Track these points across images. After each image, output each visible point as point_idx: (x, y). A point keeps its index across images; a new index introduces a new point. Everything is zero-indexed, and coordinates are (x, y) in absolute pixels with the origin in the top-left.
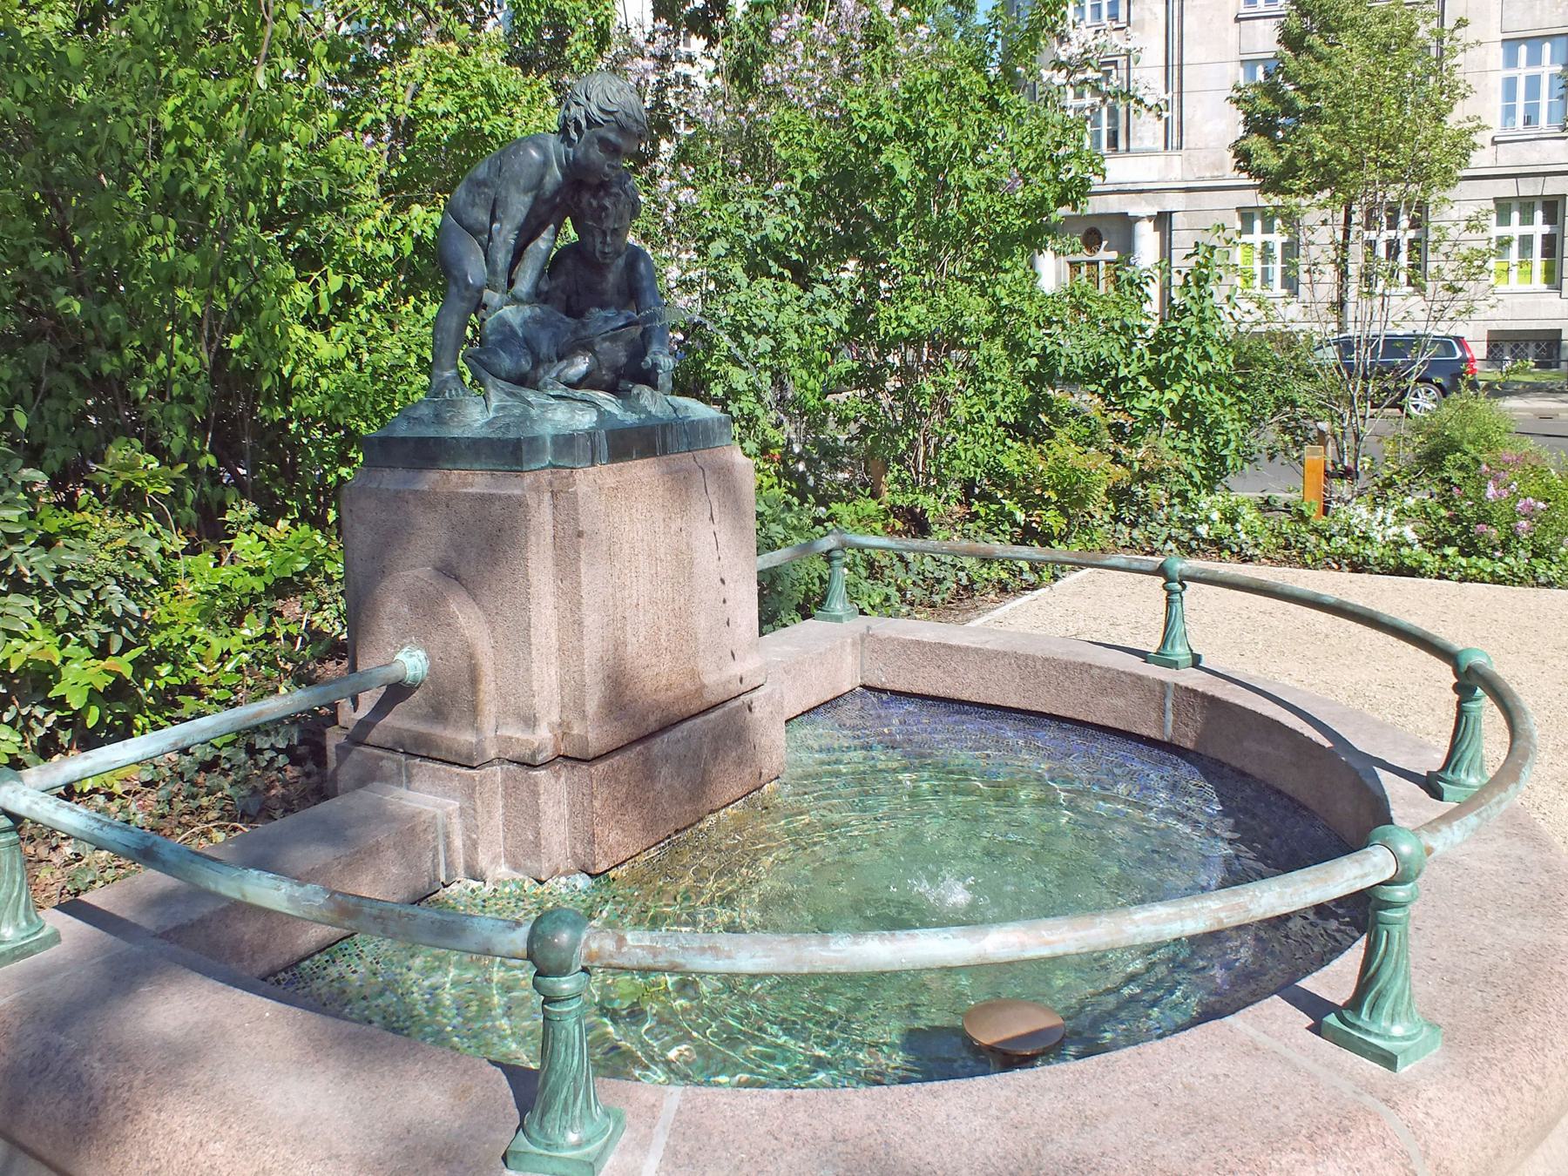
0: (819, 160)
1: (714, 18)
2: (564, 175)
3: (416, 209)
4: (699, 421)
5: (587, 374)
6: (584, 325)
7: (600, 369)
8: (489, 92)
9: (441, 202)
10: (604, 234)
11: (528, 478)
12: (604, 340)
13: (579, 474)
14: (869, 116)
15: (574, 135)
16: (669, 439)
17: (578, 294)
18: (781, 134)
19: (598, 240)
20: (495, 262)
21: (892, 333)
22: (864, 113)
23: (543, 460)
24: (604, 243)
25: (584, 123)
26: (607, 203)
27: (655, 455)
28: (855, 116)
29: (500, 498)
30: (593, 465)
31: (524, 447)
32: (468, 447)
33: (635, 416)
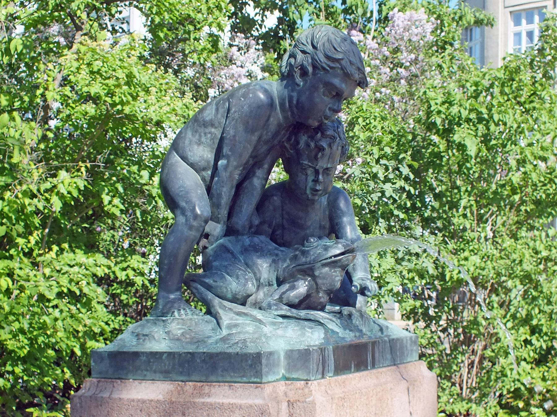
0: (393, 140)
1: (282, 38)
2: (285, 118)
3: (63, 174)
4: (398, 339)
5: (308, 296)
6: (304, 253)
7: (318, 292)
8: (130, 79)
9: (83, 170)
10: (317, 172)
11: (268, 389)
12: (324, 265)
13: (314, 385)
14: (443, 103)
15: (299, 80)
16: (377, 355)
17: (283, 227)
18: (360, 120)
19: (311, 178)
20: (220, 196)
21: (455, 277)
22: (439, 101)
23: (278, 373)
24: (316, 181)
25: (310, 69)
26: (324, 144)
27: (366, 368)
28: (432, 103)
29: (240, 407)
30: (323, 377)
31: (264, 361)
32: (204, 361)
33: (352, 334)
